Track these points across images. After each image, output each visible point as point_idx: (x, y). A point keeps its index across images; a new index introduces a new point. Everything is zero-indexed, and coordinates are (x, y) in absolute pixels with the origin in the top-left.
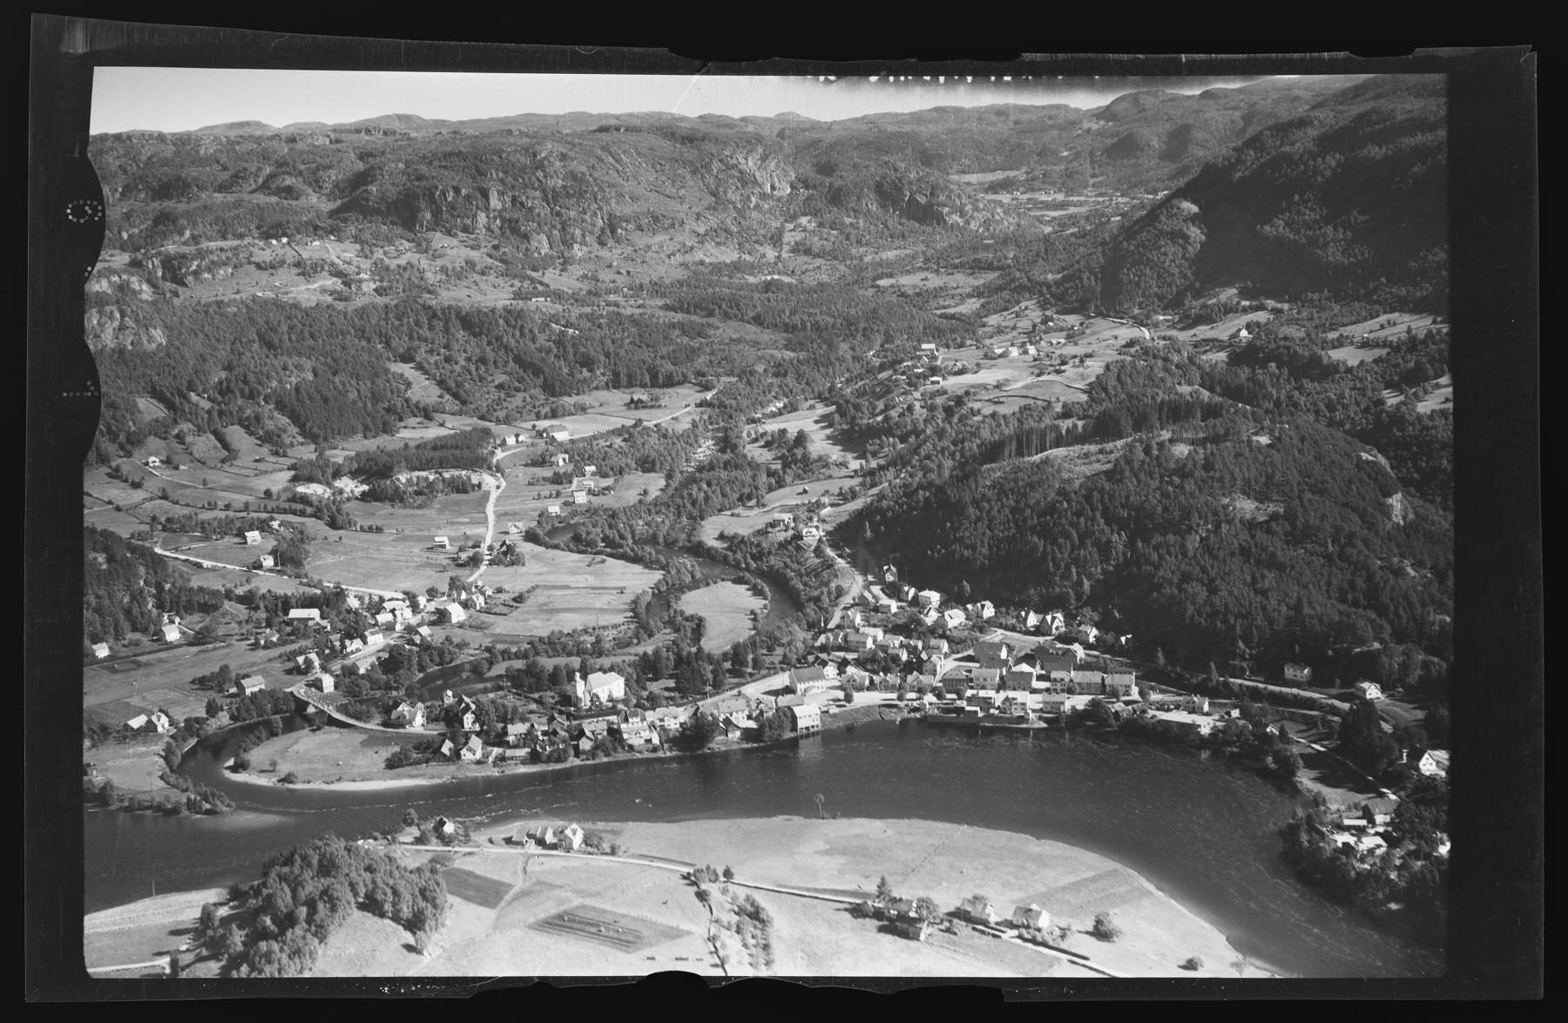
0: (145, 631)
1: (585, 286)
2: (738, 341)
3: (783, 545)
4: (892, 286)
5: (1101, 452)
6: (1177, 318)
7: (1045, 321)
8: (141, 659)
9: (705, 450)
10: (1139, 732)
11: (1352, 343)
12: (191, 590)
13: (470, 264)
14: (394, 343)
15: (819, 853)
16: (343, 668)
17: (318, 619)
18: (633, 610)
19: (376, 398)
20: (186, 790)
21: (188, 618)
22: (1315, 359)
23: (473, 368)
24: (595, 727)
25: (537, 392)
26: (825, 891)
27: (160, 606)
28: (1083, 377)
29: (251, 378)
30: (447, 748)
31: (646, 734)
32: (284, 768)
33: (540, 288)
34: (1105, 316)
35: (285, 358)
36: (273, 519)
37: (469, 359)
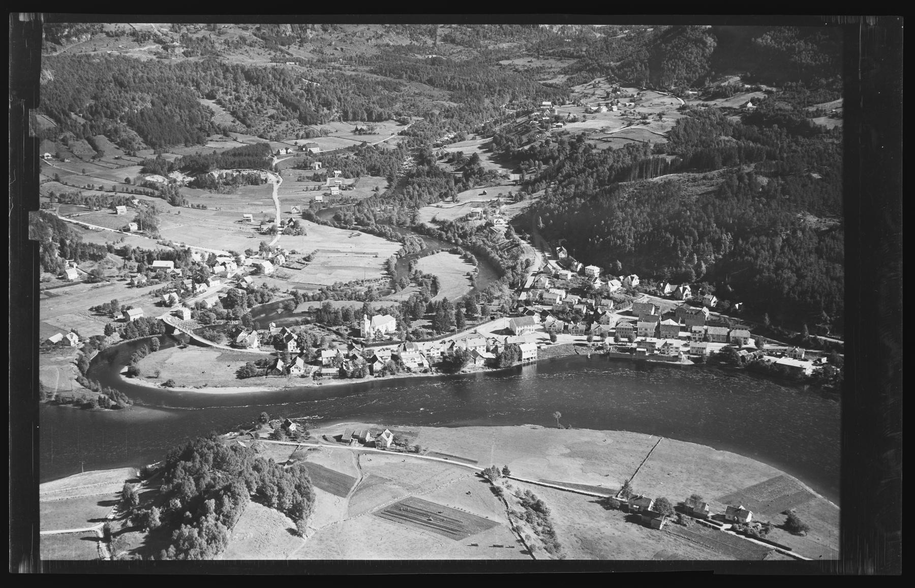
0: (53, 272)
1: (315, 57)
2: (420, 94)
3: (480, 229)
4: (510, 65)
5: (704, 178)
6: (700, 93)
7: (615, 91)
8: (51, 291)
9: (408, 162)
10: (757, 369)
11: (825, 115)
12: (84, 245)
13: (243, 39)
14: (202, 87)
15: (562, 455)
16: (196, 304)
17: (172, 268)
18: (387, 269)
19: (192, 120)
20: (96, 390)
21: (83, 264)
22: (805, 124)
23: (254, 104)
24: (383, 354)
25: (295, 121)
26: (577, 486)
27: (63, 254)
28: (662, 127)
29: (112, 105)
30: (280, 365)
31: (419, 361)
32: (165, 376)
33: (287, 56)
34: (653, 90)
35: (133, 93)
36: (134, 198)
37: (251, 99)
